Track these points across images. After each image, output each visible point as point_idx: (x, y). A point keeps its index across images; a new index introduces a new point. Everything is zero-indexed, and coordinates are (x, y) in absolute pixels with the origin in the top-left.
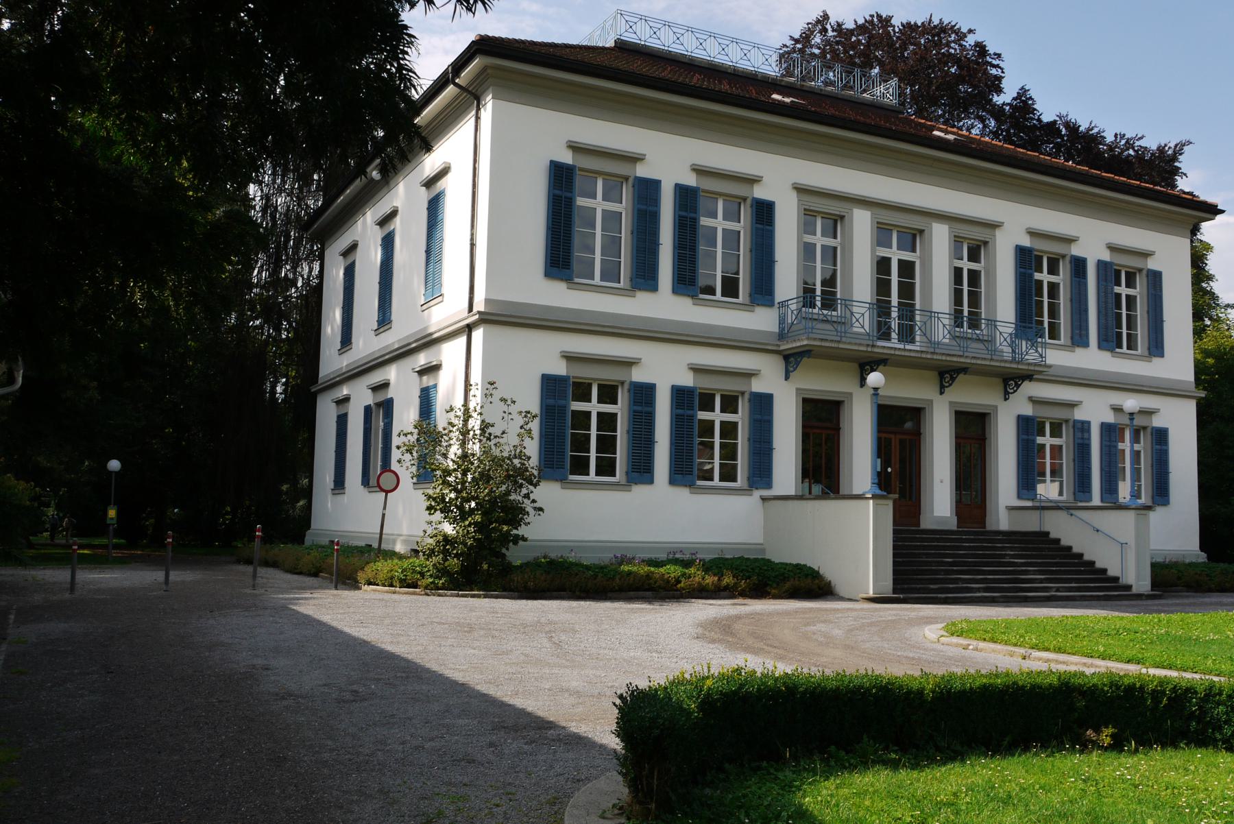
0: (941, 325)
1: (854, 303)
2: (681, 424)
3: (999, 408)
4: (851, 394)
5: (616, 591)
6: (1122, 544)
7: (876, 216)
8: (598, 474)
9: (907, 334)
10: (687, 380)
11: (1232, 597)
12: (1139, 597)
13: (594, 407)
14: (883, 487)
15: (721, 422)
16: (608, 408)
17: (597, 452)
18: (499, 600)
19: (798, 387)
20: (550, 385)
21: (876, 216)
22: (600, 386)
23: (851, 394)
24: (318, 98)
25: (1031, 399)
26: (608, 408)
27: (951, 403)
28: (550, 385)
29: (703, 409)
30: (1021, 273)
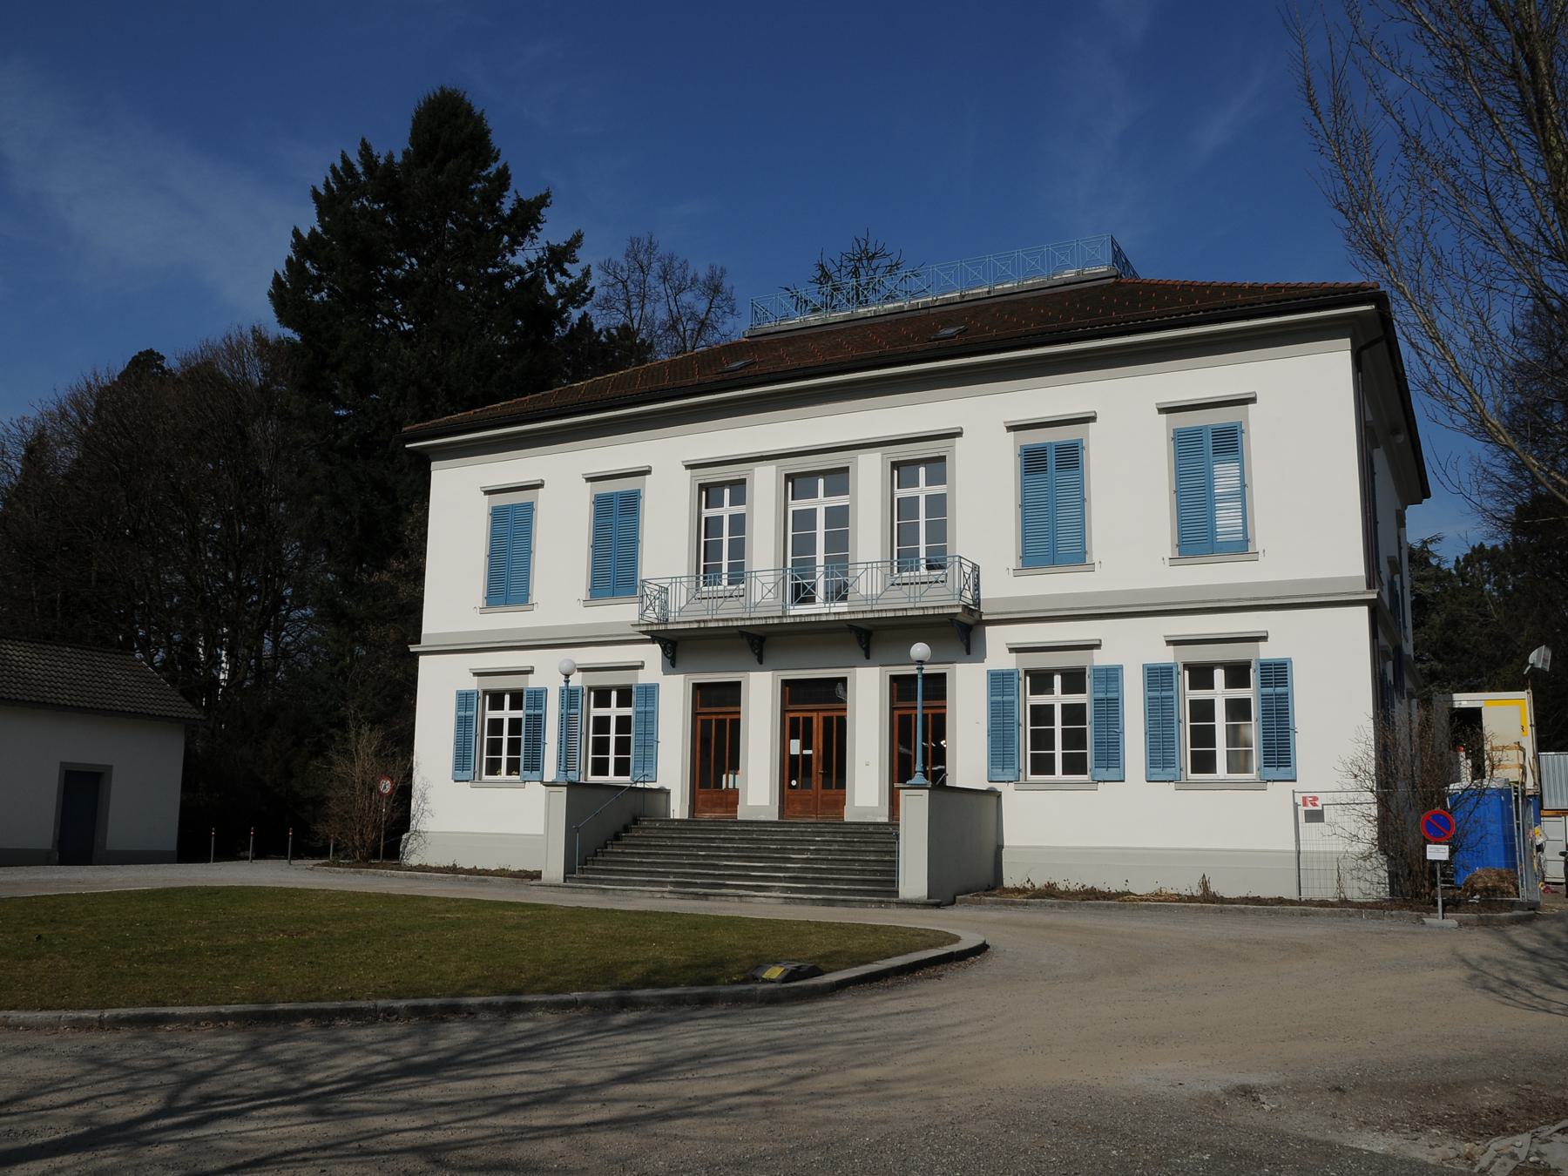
0: (759, 585)
7: (783, 468)
8: (617, 774)
9: (839, 592)
10: (473, 684)
13: (1057, 698)
15: (617, 717)
16: (1238, 693)
20: (464, 699)
21: (783, 468)
26: (1238, 693)
28: (464, 699)
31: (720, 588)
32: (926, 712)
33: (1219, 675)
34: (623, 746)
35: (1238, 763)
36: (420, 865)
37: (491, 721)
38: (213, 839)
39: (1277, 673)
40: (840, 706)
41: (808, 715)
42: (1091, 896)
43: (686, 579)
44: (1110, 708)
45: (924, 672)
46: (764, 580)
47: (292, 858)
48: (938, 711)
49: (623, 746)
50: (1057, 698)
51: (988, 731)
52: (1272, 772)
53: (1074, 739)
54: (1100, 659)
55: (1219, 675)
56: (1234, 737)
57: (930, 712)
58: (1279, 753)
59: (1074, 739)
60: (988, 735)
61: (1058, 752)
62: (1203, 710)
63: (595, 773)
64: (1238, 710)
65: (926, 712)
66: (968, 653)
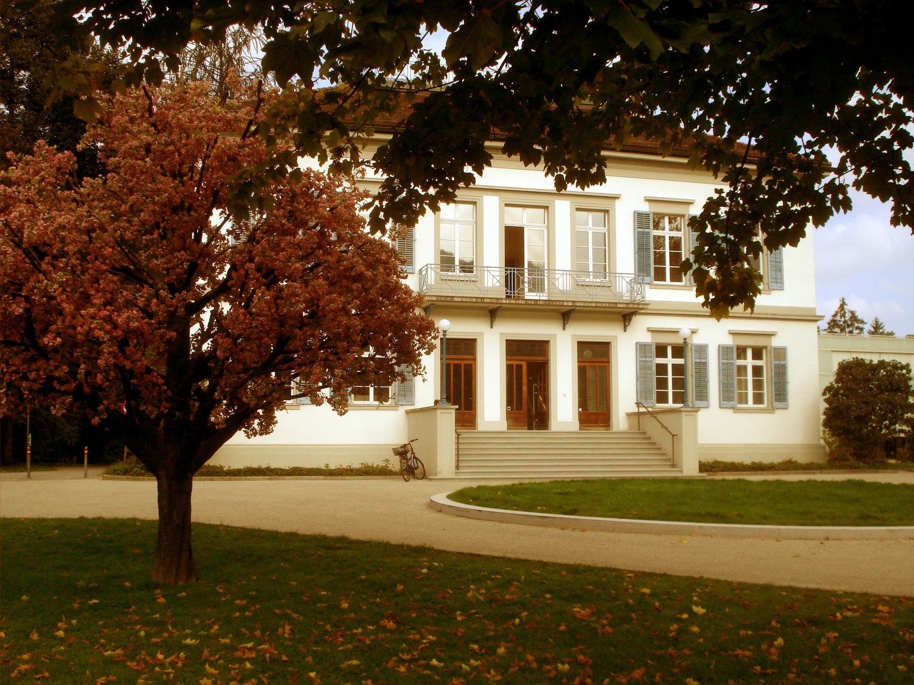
0: (490, 277)
1: (557, 272)
2: (725, 371)
3: (618, 338)
4: (482, 333)
5: (395, 474)
6: (673, 435)
8: (674, 402)
10: (729, 341)
11: (909, 469)
12: (395, 474)
14: (452, 399)
15: (673, 365)
16: (758, 363)
17: (754, 389)
18: (76, 481)
19: (573, 333)
22: (673, 348)
23: (555, 335)
24: (451, 160)
25: (649, 330)
26: (758, 363)
27: (501, 334)
29: (739, 357)
30: (639, 232)
31: (454, 274)
32: (449, 362)
33: (749, 353)
34: (662, 383)
35: (758, 399)
36: (753, 463)
37: (658, 365)
38: (86, 456)
39: (781, 353)
40: (604, 359)
41: (519, 363)
42: (297, 472)
43: (433, 266)
44: (702, 368)
45: (447, 337)
46: (494, 273)
47: (32, 470)
48: (469, 362)
49: (662, 383)
50: (670, 361)
51: (637, 377)
52: (777, 404)
53: (680, 383)
54: (776, 342)
55: (749, 353)
56: (758, 385)
57: (452, 362)
58: (781, 394)
59: (680, 383)
60: (637, 380)
61: (670, 390)
62: (742, 370)
63: (658, 401)
64: (757, 371)
65: (449, 362)
66: (564, 329)
